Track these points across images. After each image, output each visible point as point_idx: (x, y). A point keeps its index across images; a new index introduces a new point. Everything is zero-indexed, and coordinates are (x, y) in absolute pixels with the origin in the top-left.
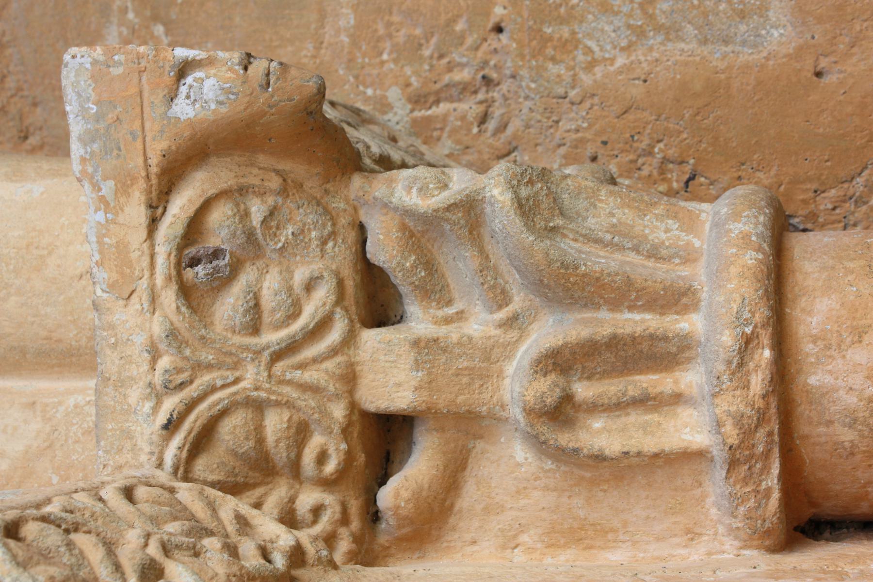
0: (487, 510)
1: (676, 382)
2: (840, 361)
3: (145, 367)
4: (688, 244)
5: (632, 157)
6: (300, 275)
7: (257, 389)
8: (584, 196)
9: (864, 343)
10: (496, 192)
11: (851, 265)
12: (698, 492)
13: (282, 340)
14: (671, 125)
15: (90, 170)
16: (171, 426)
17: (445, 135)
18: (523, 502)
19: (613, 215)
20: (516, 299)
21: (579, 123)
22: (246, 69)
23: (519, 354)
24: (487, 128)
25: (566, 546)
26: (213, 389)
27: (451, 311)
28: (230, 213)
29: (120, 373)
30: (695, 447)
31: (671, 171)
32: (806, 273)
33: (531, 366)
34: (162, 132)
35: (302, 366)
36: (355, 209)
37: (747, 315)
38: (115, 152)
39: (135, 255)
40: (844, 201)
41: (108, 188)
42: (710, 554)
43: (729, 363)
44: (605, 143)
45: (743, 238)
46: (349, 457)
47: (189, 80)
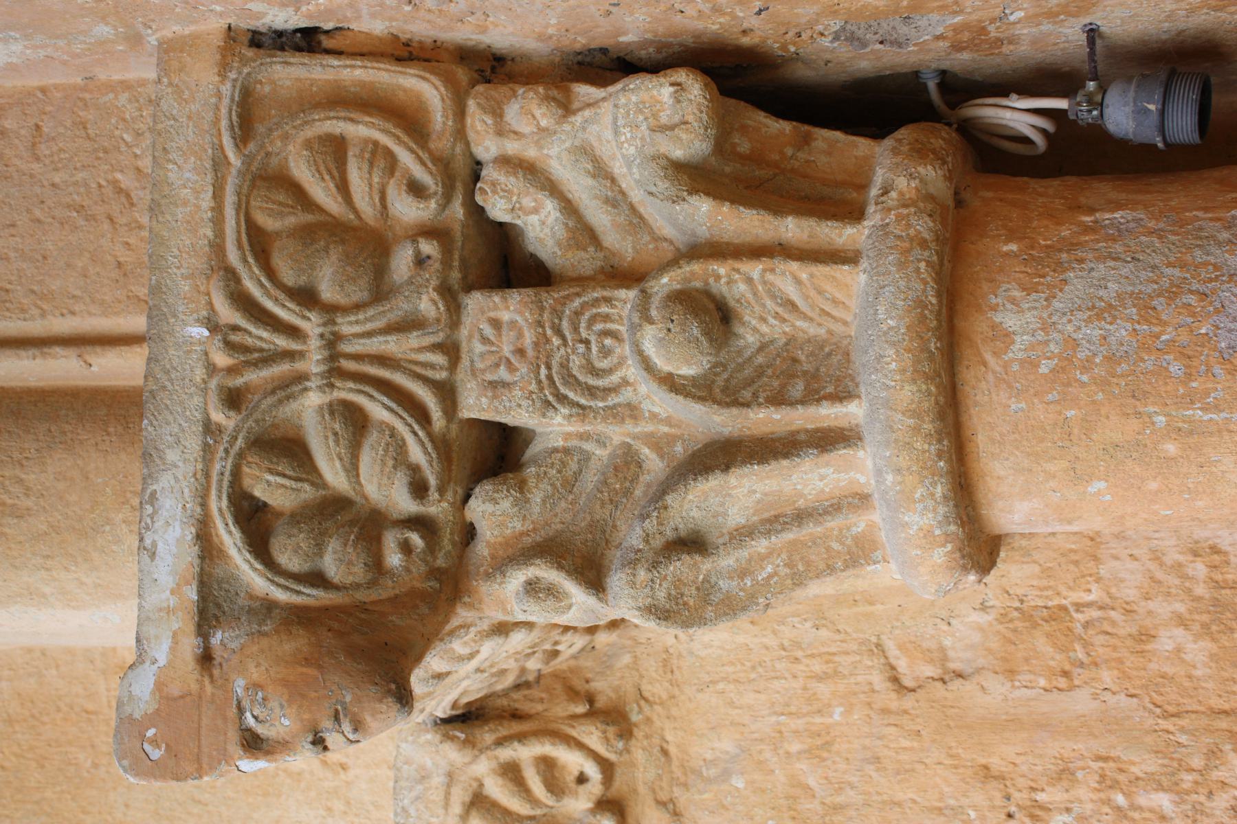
11: (1051, 467)
19: (755, 492)
32: (999, 478)
45: (925, 537)
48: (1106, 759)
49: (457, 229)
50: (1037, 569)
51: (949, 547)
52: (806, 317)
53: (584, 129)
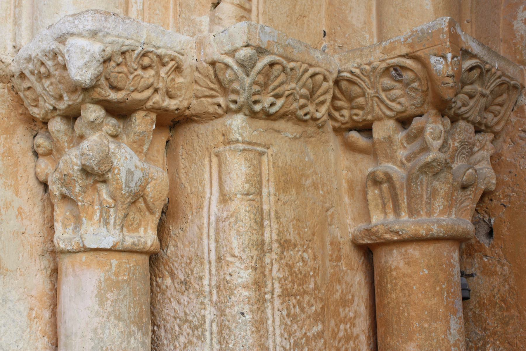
0: (356, 162)
1: (390, 213)
2: (400, 258)
3: (365, 62)
4: (435, 213)
5: (511, 185)
6: (402, 100)
7: (368, 94)
8: (446, 180)
9: (406, 265)
10: (431, 156)
11: (432, 261)
12: (364, 221)
13: (383, 99)
14: (522, 198)
15: (414, 34)
16: (352, 73)
17: (518, 119)
18: (358, 172)
20: (410, 164)
21: (522, 166)
22: (448, 76)
23: (394, 167)
24: (521, 133)
25: (348, 185)
26: (364, 82)
27: (405, 145)
28: (412, 77)
29: (363, 55)
30: (371, 220)
31: (507, 199)
33: (386, 172)
34: (426, 54)
35: (378, 105)
36: (427, 112)
37: (404, 232)
38: (419, 41)
39: (393, 53)
40: (499, 257)
41: (410, 40)
42: (350, 225)
43: (390, 228)
44: (515, 175)
46: (359, 122)
47: (442, 60)
48: (319, 270)
49: (481, 127)
50: (349, 253)
51: (424, 235)
52: (459, 206)
53: (487, 161)
